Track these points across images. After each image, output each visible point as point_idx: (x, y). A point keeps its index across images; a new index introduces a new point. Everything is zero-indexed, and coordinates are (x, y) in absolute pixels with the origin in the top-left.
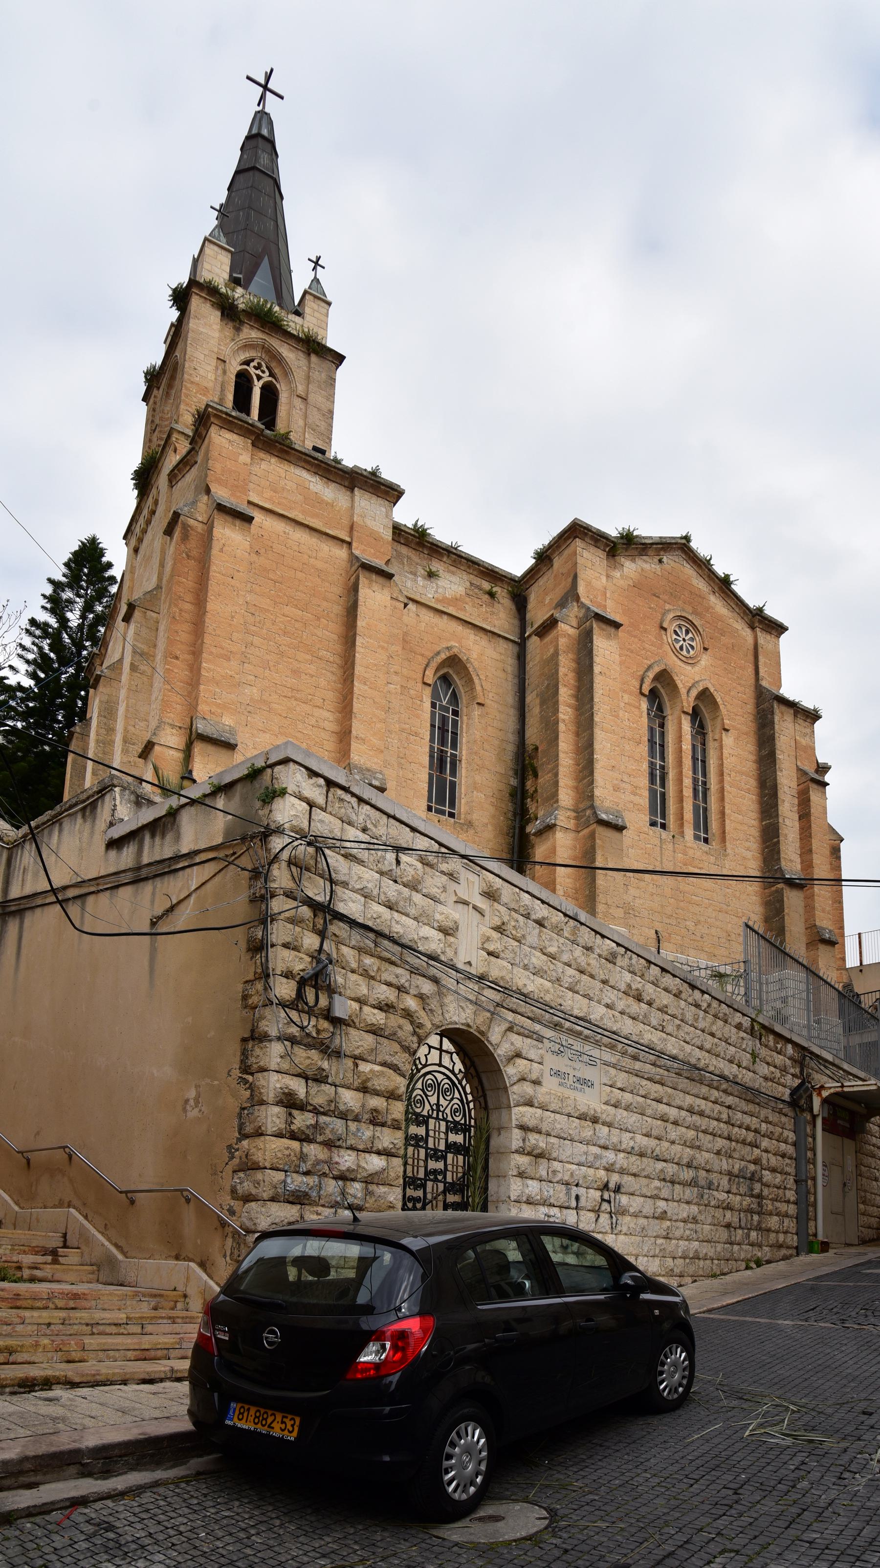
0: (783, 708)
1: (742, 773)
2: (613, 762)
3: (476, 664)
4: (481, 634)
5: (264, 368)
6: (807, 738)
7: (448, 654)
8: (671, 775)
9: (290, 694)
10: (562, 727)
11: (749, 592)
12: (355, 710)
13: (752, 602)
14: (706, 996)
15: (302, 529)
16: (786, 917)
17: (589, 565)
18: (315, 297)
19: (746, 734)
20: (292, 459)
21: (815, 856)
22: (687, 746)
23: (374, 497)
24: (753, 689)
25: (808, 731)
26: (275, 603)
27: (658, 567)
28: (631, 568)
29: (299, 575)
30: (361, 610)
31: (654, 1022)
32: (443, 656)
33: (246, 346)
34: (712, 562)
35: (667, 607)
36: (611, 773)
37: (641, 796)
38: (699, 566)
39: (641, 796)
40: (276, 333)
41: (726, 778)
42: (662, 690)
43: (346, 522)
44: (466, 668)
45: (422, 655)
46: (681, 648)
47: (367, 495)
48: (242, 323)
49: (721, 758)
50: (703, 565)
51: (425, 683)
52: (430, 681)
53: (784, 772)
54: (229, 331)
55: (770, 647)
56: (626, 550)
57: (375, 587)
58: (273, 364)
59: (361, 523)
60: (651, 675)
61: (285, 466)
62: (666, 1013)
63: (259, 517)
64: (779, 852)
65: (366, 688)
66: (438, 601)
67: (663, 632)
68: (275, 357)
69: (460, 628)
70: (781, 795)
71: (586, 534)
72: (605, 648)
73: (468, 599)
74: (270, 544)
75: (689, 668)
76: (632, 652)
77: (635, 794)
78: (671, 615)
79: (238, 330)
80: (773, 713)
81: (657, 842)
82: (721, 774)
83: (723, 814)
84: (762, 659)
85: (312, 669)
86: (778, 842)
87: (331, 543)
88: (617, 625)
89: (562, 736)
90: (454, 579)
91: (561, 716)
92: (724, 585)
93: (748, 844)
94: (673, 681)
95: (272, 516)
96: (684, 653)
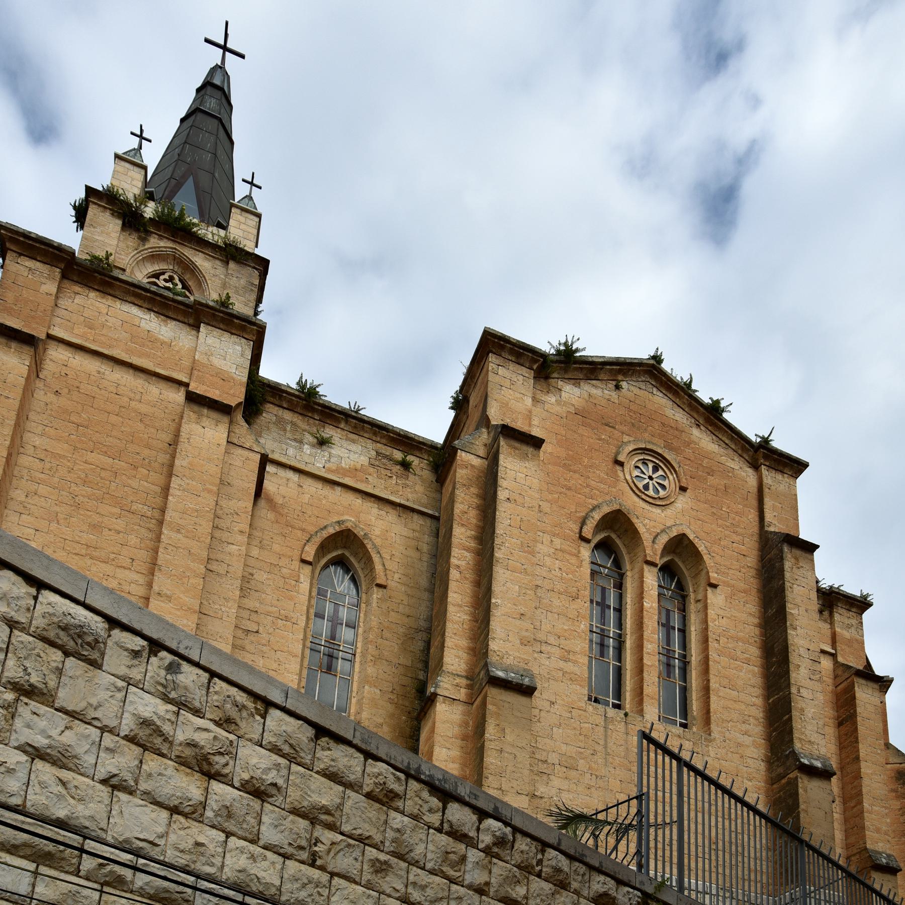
0: (798, 552)
1: (738, 639)
2: (523, 610)
3: (378, 541)
4: (389, 508)
5: (177, 280)
6: (853, 630)
7: (338, 529)
8: (629, 643)
9: (83, 552)
10: (454, 574)
11: (747, 421)
12: (159, 562)
13: (752, 431)
14: (490, 822)
15: (124, 369)
16: (802, 815)
17: (508, 383)
18: (243, 210)
19: (745, 592)
20: (117, 293)
21: (863, 764)
22: (651, 603)
23: (227, 335)
24: (756, 538)
25: (854, 622)
26: (75, 448)
27: (614, 395)
28: (572, 393)
29: (113, 419)
30: (183, 446)
31: (269, 834)
32: (331, 531)
33: (154, 257)
34: (694, 386)
35: (626, 439)
36: (518, 622)
37: (575, 662)
38: (676, 393)
39: (575, 662)
40: (190, 242)
41: (712, 645)
42: (618, 541)
43: (186, 363)
44: (363, 546)
45: (303, 530)
46: (646, 487)
47: (217, 332)
48: (148, 233)
49: (705, 621)
50: (681, 392)
51: (303, 561)
52: (310, 559)
53: (799, 631)
54: (131, 240)
55: (782, 488)
56: (566, 371)
57: (206, 422)
58: (187, 277)
59: (205, 361)
60: (597, 516)
61: (109, 301)
62: (331, 827)
63: (56, 354)
64: (791, 732)
65: (180, 536)
66: (330, 471)
67: (618, 468)
68: (188, 268)
69: (359, 501)
70: (794, 658)
71: (502, 347)
72: (514, 468)
73: (371, 470)
74: (76, 384)
75: (657, 511)
76: (569, 489)
77: (566, 660)
78: (631, 447)
79: (144, 240)
80: (782, 559)
81: (600, 720)
82: (705, 640)
83: (706, 690)
84: (768, 503)
85: (120, 524)
86: (790, 719)
87: (163, 385)
88: (537, 443)
89: (453, 585)
90: (353, 447)
91: (454, 561)
92: (712, 415)
93: (745, 727)
94: (632, 524)
95: (82, 354)
96: (651, 492)
